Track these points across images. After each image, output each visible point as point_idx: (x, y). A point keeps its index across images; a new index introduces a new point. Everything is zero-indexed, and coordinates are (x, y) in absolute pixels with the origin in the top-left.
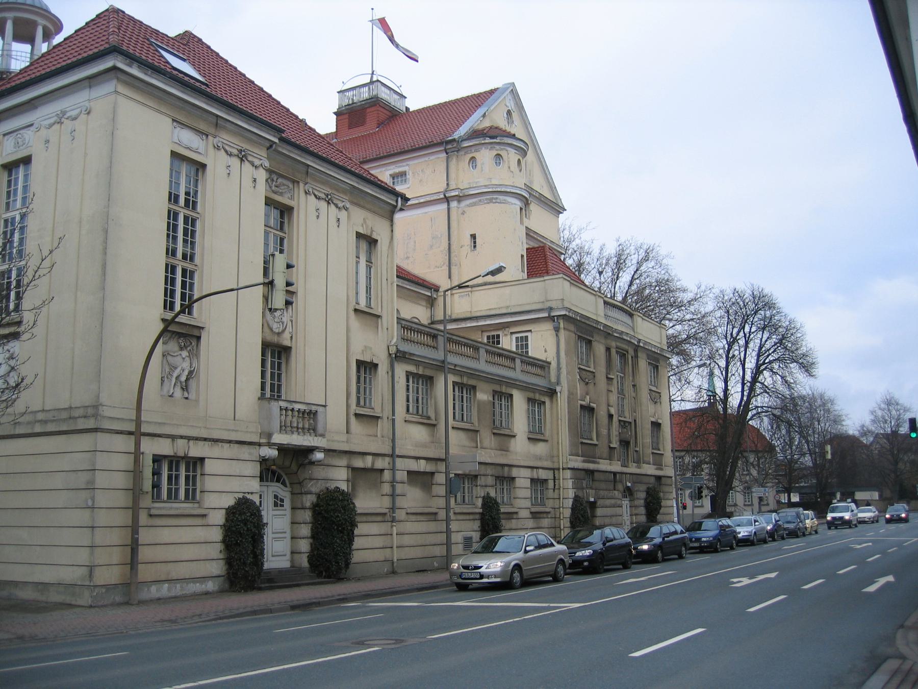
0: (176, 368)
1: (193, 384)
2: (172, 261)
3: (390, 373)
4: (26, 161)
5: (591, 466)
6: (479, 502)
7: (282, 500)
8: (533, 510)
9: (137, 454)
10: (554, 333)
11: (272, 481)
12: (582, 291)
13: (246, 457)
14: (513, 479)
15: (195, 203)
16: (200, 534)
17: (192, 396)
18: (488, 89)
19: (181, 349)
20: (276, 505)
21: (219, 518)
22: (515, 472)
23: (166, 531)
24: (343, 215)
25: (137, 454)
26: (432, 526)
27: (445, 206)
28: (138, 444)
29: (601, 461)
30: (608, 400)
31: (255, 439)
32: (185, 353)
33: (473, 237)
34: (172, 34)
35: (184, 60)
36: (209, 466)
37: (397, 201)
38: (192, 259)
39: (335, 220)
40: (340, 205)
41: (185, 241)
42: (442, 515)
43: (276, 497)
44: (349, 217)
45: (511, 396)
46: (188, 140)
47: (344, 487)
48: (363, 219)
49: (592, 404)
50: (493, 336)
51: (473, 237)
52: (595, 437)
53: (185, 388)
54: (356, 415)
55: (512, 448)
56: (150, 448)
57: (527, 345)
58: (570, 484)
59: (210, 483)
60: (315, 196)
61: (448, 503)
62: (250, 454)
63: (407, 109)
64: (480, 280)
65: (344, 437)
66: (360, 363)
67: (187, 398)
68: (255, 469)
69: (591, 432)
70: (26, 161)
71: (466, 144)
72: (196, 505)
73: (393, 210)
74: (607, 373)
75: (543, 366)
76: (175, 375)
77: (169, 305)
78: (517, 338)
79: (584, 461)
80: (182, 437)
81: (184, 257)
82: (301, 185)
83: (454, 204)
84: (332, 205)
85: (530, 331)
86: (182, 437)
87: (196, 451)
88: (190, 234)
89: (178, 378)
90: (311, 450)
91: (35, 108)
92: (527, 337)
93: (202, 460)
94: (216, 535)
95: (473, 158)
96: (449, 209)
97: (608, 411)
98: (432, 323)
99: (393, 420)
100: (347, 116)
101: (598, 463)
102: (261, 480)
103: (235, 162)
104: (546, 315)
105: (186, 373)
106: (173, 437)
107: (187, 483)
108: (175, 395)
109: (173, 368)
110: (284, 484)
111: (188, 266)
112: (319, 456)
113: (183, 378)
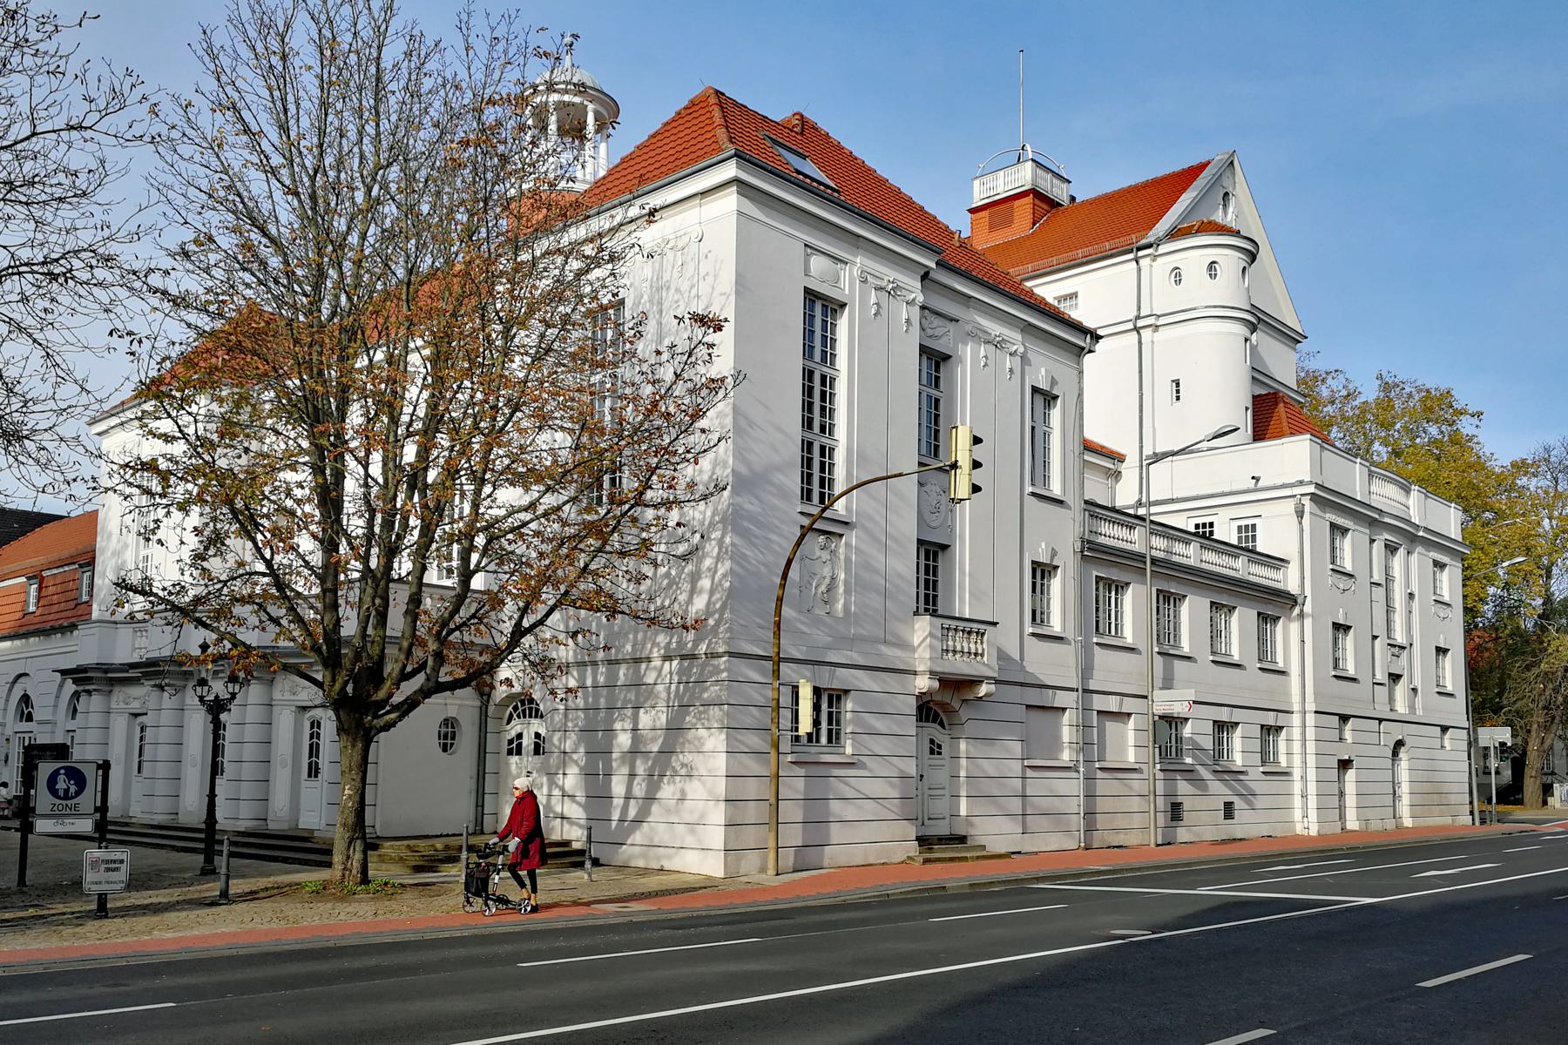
2: (809, 436)
7: (939, 746)
11: (927, 721)
18: (1194, 162)
20: (932, 752)
34: (777, 117)
35: (804, 157)
43: (932, 741)
50: (1204, 525)
57: (1254, 537)
63: (1073, 199)
64: (1205, 445)
66: (1036, 565)
68: (911, 705)
73: (1080, 352)
75: (1277, 562)
78: (1240, 527)
92: (1254, 526)
96: (1140, 342)
98: (1139, 504)
102: (920, 719)
107: (830, 723)
110: (942, 725)
112: (983, 690)
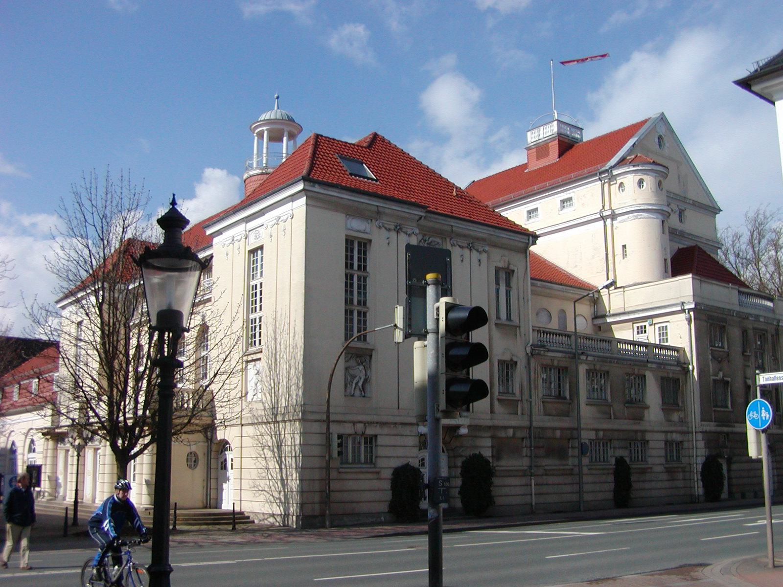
0: (355, 377)
1: (367, 386)
2: (349, 307)
3: (527, 367)
4: (261, 248)
5: (725, 429)
6: (613, 461)
8: (667, 466)
9: (328, 435)
10: (686, 322)
12: (714, 286)
13: (408, 433)
14: (648, 441)
15: (365, 267)
16: (376, 484)
17: (368, 394)
19: (359, 365)
21: (388, 474)
22: (648, 436)
23: (351, 483)
24: (484, 256)
25: (328, 435)
26: (569, 479)
27: (602, 222)
28: (328, 428)
29: (736, 424)
30: (745, 373)
31: (414, 420)
32: (361, 367)
33: (624, 247)
36: (380, 440)
37: (529, 240)
38: (365, 303)
39: (477, 261)
40: (481, 249)
41: (359, 293)
42: (576, 470)
44: (488, 257)
45: (645, 376)
46: (358, 225)
47: (487, 453)
48: (499, 258)
49: (725, 379)
50: (641, 327)
51: (624, 247)
52: (730, 406)
53: (363, 388)
54: (498, 399)
55: (646, 417)
56: (335, 429)
58: (701, 444)
59: (381, 452)
60: (460, 246)
61: (580, 461)
62: (411, 431)
65: (489, 416)
67: (364, 396)
69: (726, 400)
70: (261, 248)
71: (615, 172)
72: (373, 466)
74: (744, 352)
76: (355, 382)
77: (348, 335)
79: (717, 426)
80: (360, 422)
81: (359, 303)
82: (448, 240)
83: (609, 221)
84: (474, 251)
85: (669, 321)
86: (360, 422)
87: (370, 431)
88: (363, 288)
89: (357, 384)
90: (458, 427)
91: (264, 214)
93: (376, 436)
94: (387, 485)
95: (622, 183)
97: (745, 382)
99: (531, 402)
100: (535, 150)
101: (734, 427)
103: (393, 234)
104: (679, 308)
105: (362, 380)
106: (354, 423)
108: (356, 394)
109: (353, 377)
111: (363, 309)
113: (360, 384)
